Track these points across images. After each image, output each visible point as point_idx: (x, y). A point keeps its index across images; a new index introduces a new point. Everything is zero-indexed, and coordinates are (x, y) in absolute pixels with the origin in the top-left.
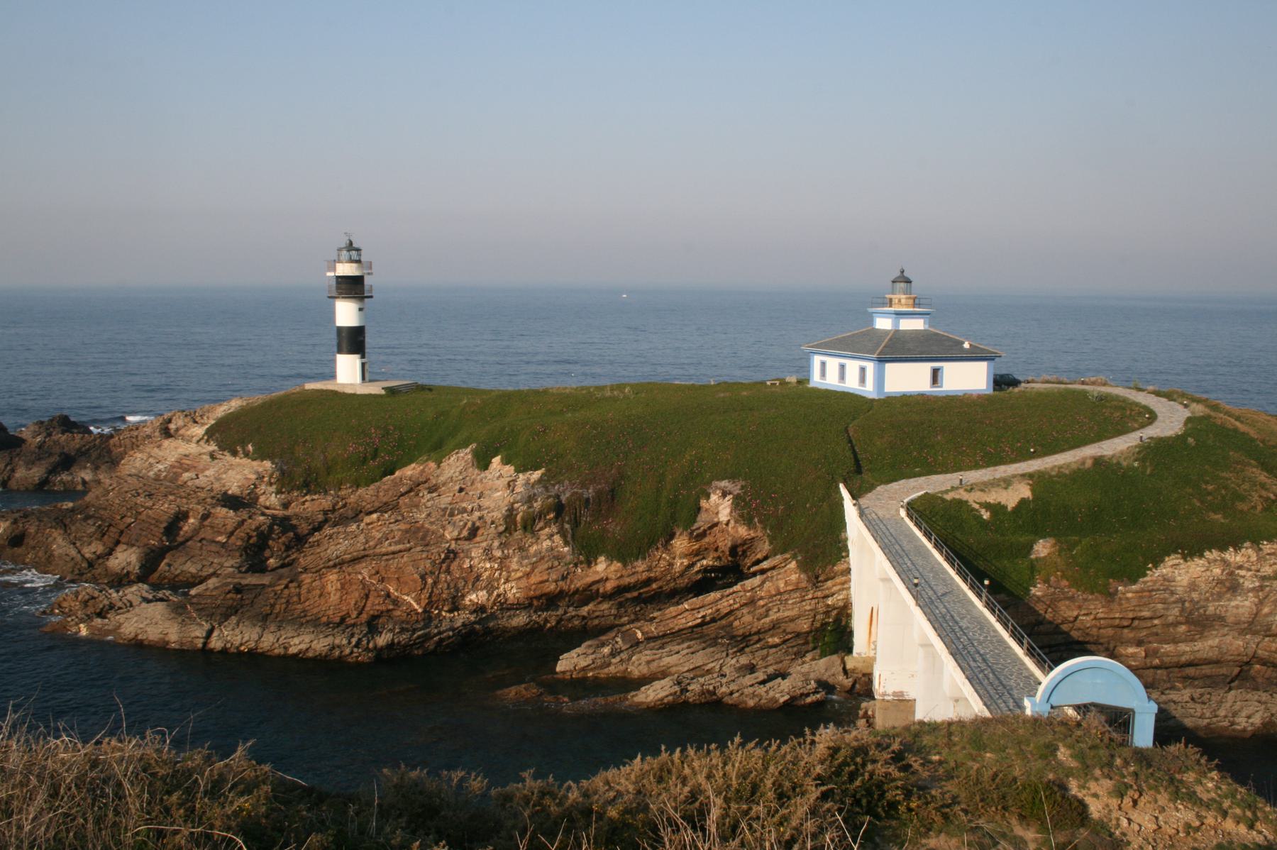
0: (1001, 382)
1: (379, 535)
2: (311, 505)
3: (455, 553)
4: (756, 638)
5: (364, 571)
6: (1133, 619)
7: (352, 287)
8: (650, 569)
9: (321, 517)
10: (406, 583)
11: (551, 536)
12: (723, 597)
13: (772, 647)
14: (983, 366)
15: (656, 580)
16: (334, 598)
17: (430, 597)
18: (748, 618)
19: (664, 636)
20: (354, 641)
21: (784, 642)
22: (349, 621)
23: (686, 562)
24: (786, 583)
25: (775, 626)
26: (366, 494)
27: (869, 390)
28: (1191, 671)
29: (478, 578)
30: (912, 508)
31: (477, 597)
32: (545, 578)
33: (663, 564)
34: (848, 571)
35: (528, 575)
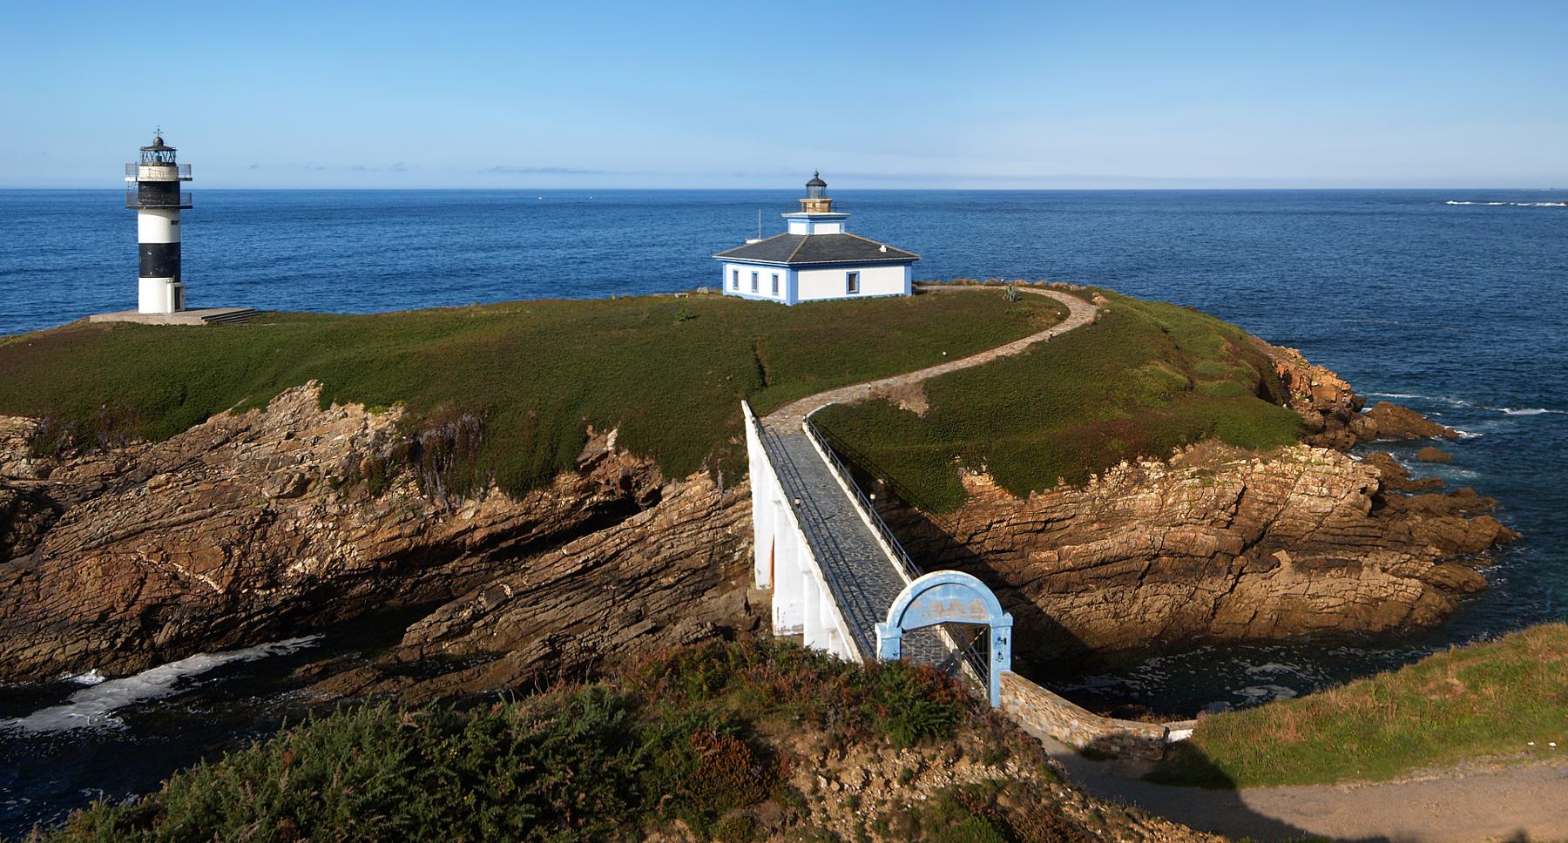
0: (916, 287)
1: (166, 502)
2: (86, 469)
3: (275, 516)
4: (647, 580)
5: (142, 549)
6: (1047, 522)
7: (164, 195)
8: (528, 512)
9: (97, 484)
10: (202, 558)
11: (405, 484)
12: (608, 536)
13: (666, 588)
14: (902, 269)
15: (536, 523)
16: (91, 589)
17: (237, 573)
18: (637, 558)
19: (539, 588)
20: (119, 642)
21: (679, 581)
22: (113, 617)
23: (572, 500)
24: (680, 515)
25: (668, 565)
26: (165, 450)
27: (783, 297)
28: (1102, 570)
29: (306, 542)
30: (813, 422)
31: (303, 566)
32: (396, 533)
33: (544, 503)
34: (749, 495)
35: (373, 532)
